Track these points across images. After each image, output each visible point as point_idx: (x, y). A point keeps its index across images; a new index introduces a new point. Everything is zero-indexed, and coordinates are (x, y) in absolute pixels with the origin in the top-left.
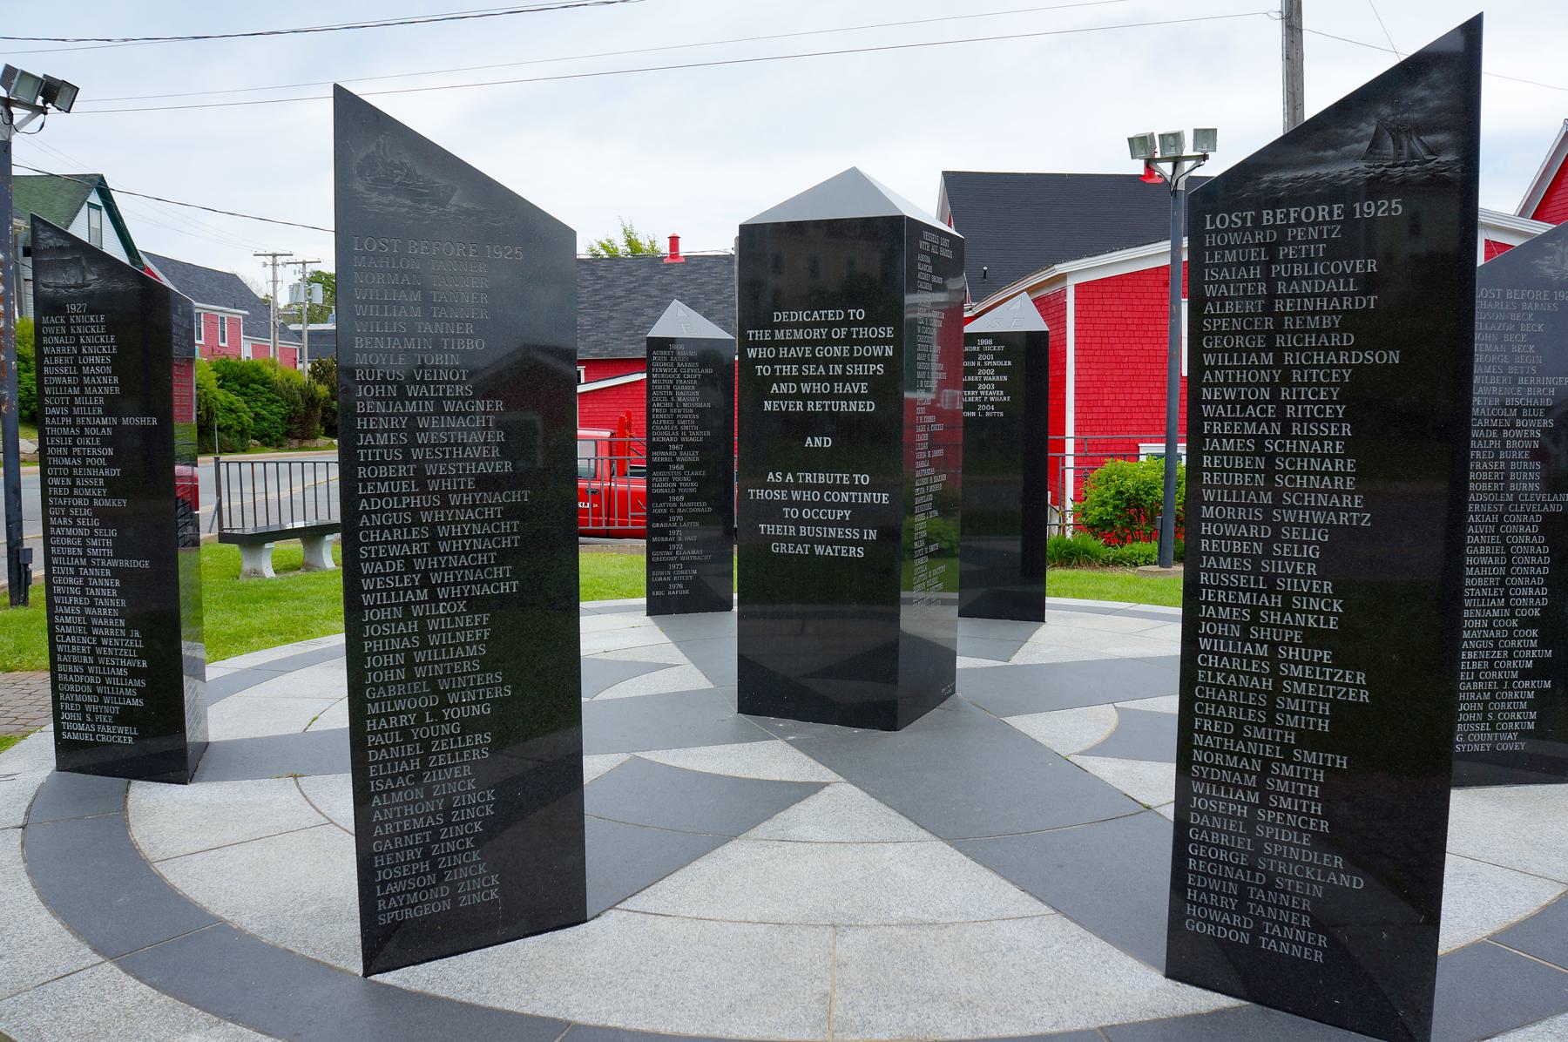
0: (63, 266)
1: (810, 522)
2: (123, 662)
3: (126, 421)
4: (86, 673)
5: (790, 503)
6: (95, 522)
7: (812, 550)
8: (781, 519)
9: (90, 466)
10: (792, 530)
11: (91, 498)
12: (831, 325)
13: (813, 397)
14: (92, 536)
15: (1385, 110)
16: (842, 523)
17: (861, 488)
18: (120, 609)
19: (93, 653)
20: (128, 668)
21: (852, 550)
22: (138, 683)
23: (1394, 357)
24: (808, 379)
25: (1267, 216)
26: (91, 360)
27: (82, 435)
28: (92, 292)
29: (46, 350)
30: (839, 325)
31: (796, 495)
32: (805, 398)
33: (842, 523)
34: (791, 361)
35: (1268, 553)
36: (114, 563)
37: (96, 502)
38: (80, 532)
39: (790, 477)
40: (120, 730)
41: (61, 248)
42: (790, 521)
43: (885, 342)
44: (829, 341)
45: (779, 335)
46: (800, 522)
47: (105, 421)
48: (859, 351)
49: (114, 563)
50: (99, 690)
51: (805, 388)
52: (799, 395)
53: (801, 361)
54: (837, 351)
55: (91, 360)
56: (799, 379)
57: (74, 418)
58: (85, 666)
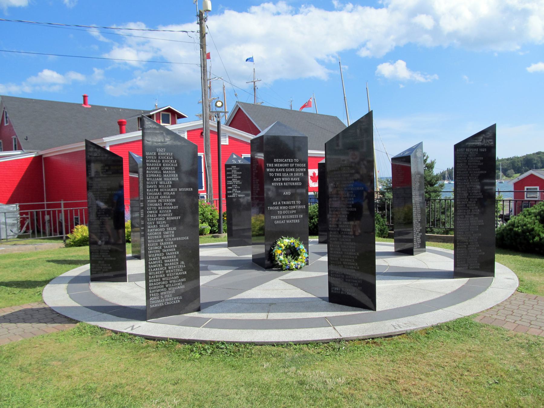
0: (156, 134)
1: (285, 214)
2: (177, 274)
3: (180, 190)
4: (162, 281)
5: (280, 210)
6: (167, 225)
7: (286, 222)
8: (277, 214)
9: (166, 206)
10: (280, 217)
11: (166, 217)
12: (290, 163)
13: (285, 182)
14: (166, 230)
15: (484, 135)
16: (294, 214)
17: (298, 205)
18: (176, 255)
19: (165, 273)
20: (179, 275)
21: (296, 221)
22: (183, 280)
23: (486, 172)
24: (284, 177)
25: (467, 150)
26: (167, 168)
27: (163, 195)
28: (168, 145)
29: (147, 165)
30: (292, 163)
31: (281, 208)
32: (283, 182)
33: (294, 214)
34: (279, 172)
35: (468, 203)
36: (175, 239)
37: (168, 218)
38: (161, 230)
39: (279, 203)
40: (175, 298)
41: (155, 128)
42: (280, 215)
43: (303, 168)
44: (289, 167)
45: (276, 165)
46: (283, 214)
47: (172, 190)
48: (297, 170)
49: (175, 239)
50: (167, 286)
51: (283, 179)
52: (282, 181)
53: (282, 172)
54: (291, 170)
55: (167, 168)
56: (281, 177)
57: (159, 189)
58: (161, 278)
